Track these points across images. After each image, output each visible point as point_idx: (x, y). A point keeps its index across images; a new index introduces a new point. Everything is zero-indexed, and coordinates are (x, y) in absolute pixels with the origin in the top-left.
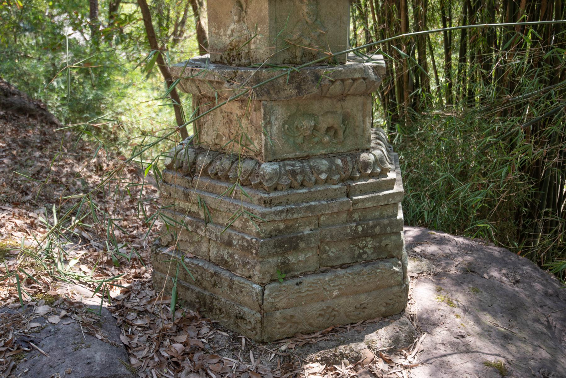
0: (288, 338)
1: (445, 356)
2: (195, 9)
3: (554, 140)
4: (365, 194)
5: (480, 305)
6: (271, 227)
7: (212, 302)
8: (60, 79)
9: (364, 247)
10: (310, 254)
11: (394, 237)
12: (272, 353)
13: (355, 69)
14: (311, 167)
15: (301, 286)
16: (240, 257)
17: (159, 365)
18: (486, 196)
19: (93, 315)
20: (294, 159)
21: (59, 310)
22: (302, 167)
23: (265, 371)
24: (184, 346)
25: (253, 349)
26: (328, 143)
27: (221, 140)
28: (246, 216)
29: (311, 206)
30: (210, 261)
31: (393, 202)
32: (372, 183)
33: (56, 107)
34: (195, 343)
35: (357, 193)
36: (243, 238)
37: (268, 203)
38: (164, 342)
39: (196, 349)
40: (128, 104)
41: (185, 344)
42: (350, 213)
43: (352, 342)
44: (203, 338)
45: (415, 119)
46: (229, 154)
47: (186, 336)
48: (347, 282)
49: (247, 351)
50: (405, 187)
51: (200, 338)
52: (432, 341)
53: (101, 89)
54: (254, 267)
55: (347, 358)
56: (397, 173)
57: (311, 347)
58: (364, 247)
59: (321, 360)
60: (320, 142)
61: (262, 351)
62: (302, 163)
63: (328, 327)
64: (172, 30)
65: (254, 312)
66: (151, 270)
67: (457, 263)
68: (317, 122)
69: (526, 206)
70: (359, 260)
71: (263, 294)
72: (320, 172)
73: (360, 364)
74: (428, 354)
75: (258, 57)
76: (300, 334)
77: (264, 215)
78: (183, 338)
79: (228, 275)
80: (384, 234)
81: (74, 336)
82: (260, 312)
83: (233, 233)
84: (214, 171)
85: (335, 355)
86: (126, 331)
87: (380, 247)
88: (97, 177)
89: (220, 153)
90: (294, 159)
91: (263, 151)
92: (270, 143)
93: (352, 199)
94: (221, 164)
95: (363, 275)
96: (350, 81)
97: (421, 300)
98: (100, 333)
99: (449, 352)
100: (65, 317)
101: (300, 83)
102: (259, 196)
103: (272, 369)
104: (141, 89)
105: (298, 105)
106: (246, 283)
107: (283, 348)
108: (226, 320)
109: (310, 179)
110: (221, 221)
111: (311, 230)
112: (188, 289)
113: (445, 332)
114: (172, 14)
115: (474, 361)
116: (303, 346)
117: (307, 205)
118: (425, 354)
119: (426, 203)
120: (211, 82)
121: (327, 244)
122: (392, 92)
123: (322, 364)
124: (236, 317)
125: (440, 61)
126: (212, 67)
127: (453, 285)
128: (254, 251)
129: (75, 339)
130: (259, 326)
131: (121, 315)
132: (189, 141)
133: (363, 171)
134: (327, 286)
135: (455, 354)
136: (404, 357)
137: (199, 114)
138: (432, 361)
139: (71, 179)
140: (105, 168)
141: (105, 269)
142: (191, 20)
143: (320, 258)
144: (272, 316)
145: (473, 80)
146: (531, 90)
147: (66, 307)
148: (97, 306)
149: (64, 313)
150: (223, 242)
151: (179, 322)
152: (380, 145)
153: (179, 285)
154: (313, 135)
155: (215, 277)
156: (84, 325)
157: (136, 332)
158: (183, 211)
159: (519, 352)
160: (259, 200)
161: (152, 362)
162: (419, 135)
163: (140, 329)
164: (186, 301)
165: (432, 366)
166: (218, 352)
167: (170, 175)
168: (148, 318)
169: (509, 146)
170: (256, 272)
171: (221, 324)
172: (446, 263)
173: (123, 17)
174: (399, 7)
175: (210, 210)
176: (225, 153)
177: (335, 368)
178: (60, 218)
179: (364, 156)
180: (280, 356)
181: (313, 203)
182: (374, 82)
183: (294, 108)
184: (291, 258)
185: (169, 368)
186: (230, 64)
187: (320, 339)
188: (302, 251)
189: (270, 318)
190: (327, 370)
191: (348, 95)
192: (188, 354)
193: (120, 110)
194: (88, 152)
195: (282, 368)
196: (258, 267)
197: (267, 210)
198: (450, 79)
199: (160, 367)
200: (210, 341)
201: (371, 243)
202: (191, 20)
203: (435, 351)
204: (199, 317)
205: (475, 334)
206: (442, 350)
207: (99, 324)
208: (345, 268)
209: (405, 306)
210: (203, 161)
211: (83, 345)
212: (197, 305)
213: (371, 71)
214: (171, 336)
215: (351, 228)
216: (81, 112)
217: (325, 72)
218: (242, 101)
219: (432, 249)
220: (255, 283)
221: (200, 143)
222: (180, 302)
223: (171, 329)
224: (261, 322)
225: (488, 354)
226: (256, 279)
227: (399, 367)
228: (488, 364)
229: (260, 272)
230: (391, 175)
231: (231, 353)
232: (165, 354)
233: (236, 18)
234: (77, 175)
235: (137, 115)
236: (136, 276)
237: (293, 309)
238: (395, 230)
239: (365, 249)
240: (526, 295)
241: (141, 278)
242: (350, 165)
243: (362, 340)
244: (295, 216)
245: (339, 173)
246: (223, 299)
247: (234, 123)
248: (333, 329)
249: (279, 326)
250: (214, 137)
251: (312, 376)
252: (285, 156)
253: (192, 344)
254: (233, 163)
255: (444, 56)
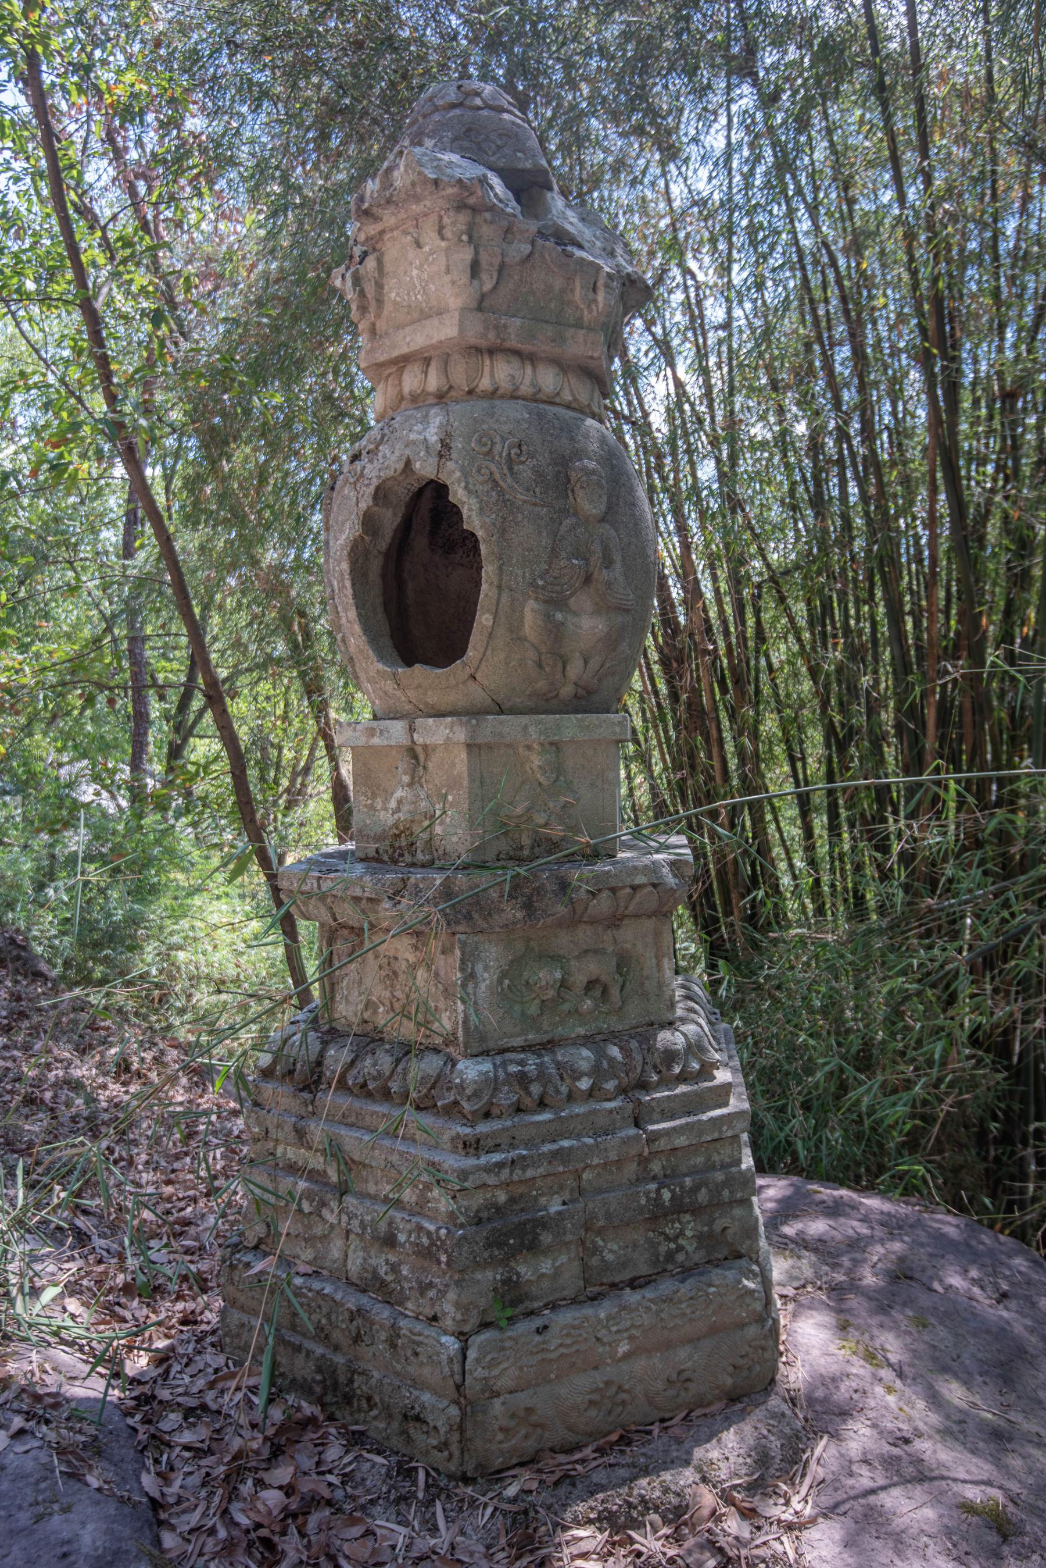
0: (521, 1464)
1: (873, 1491)
2: (330, 747)
3: (1029, 987)
4: (672, 1118)
5: (935, 1360)
6: (478, 1200)
7: (351, 1381)
8: (60, 884)
9: (677, 1237)
10: (563, 1259)
11: (738, 1212)
12: (486, 1505)
13: (635, 868)
14: (559, 1065)
15: (547, 1336)
16: (413, 1272)
17: (228, 1548)
18: (914, 1106)
19: (85, 1426)
20: (523, 1049)
21: (9, 1414)
22: (540, 1066)
23: (472, 1554)
24: (288, 1495)
25: (443, 1496)
26: (591, 1012)
27: (375, 1012)
28: (425, 1178)
29: (562, 1148)
30: (349, 1283)
31: (729, 1134)
32: (684, 1094)
33: (49, 939)
34: (312, 1486)
35: (656, 1116)
36: (420, 1228)
37: (472, 1146)
38: (241, 1487)
39: (314, 1502)
40: (193, 928)
41: (288, 1490)
42: (643, 1161)
43: (666, 1469)
44: (330, 1472)
45: (755, 945)
46: (391, 1043)
47: (291, 1470)
48: (647, 1320)
49: (430, 1503)
50: (752, 1099)
51: (323, 1473)
52: (842, 1455)
53: (142, 901)
54: (442, 1293)
55: (656, 1509)
56: (734, 1070)
57: (574, 1485)
58: (677, 1237)
59: (599, 1519)
60: (575, 1012)
61: (462, 1500)
62: (540, 1056)
63: (609, 1433)
64: (285, 783)
65: (445, 1403)
66: (219, 1303)
67: (875, 1259)
68: (566, 973)
69: (995, 1119)
70: (670, 1267)
71: (465, 1357)
72: (577, 1076)
73: (685, 1524)
74: (836, 1490)
75: (449, 849)
76: (548, 1454)
77: (464, 1175)
78: (283, 1474)
79: (386, 1314)
80: (718, 1204)
81: (37, 1482)
82: (457, 1403)
83: (398, 1215)
84: (361, 1080)
85: (630, 1505)
86: (157, 1461)
87: (711, 1235)
88: (117, 1086)
89: (373, 1041)
90: (523, 1049)
91: (460, 1034)
92: (473, 1018)
93: (645, 1131)
94: (375, 1064)
95: (681, 1302)
96: (628, 890)
97: (808, 1353)
98: (96, 1472)
99: (881, 1482)
100: (21, 1432)
101: (530, 898)
102: (453, 1133)
103: (488, 1547)
104: (218, 898)
105: (528, 940)
106: (426, 1332)
107: (512, 1491)
108: (382, 1425)
109: (558, 1092)
110: (372, 1189)
111: (564, 1203)
112: (298, 1349)
113: (867, 1431)
114: (288, 754)
115: (937, 1500)
116: (557, 1483)
117: (554, 1147)
118: (830, 1490)
119: (798, 1121)
120: (357, 899)
121: (600, 1232)
122: (708, 893)
123: (601, 1530)
124: (405, 1416)
125: (794, 832)
126: (359, 869)
127: (872, 1313)
128: (444, 1258)
129: (38, 1491)
130: (455, 1437)
131: (146, 1421)
132: (311, 1016)
133: (664, 1069)
134: (604, 1332)
135: (895, 1485)
136: (782, 1501)
137: (331, 965)
138: (847, 1506)
139: (65, 1093)
140: (135, 1066)
141: (118, 1304)
142: (322, 767)
143: (585, 1267)
144: (485, 1412)
145: (858, 868)
146: (970, 891)
147: (25, 1407)
148: (96, 1400)
149: (18, 1422)
150: (375, 1238)
151: (275, 1435)
152: (695, 1012)
153: (280, 1340)
154: (559, 999)
155: (359, 1321)
156: (61, 1451)
157: (178, 1464)
158: (293, 1169)
159: (1030, 1472)
160: (453, 1139)
161: (210, 1542)
162: (768, 977)
163: (187, 1454)
164: (294, 1380)
165: (848, 1521)
166: (363, 1508)
167: (268, 1088)
168: (207, 1424)
169: (945, 997)
170: (448, 1308)
171: (371, 1434)
172: (853, 1260)
173: (191, 768)
174: (707, 740)
175: (348, 1164)
176: (382, 1040)
177: (630, 1537)
178: (33, 1187)
179: (665, 1038)
180: (505, 1513)
181: (566, 1143)
182: (673, 891)
183: (520, 946)
184: (525, 1270)
185: (250, 1555)
186: (395, 862)
187: (594, 1464)
188: (546, 1251)
189: (480, 1417)
190: (613, 1544)
191: (624, 917)
192: (294, 1516)
193: (175, 939)
194: (103, 1033)
195: (510, 1545)
196: (452, 1295)
197: (471, 1162)
198: (817, 871)
199: (230, 1554)
200: (347, 1478)
201: (691, 1227)
202: (322, 767)
203: (851, 1482)
204: (321, 1418)
205: (932, 1432)
206: (865, 1478)
207: (95, 1448)
208: (641, 1287)
209: (775, 1369)
210: (337, 1057)
211: (56, 1507)
212: (318, 1389)
213: (666, 870)
214: (256, 1470)
215: (647, 1194)
216: (97, 945)
217: (578, 874)
218: (418, 934)
219: (818, 1227)
220: (445, 1333)
221: (332, 1020)
222: (279, 1381)
223: (257, 1453)
224: (461, 1429)
225: (965, 1482)
226: (448, 1323)
227: (775, 1527)
228: (968, 1507)
229: (457, 1305)
230: (723, 1076)
231: (393, 1509)
232: (243, 1520)
233: (406, 779)
234: (76, 1085)
235: (210, 948)
236: (188, 1320)
237: (531, 1391)
238: (739, 1195)
239: (681, 1241)
240: (1026, 1327)
241: (195, 1323)
242: (638, 1057)
243: (687, 1463)
244: (530, 1173)
245: (616, 1076)
246: (375, 1374)
247: (402, 977)
248: (622, 1437)
249: (500, 1436)
250: (361, 1007)
251: (579, 1563)
252: (505, 1042)
253: (305, 1490)
254: (398, 1061)
255: (799, 822)
